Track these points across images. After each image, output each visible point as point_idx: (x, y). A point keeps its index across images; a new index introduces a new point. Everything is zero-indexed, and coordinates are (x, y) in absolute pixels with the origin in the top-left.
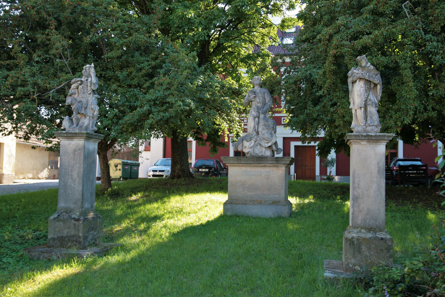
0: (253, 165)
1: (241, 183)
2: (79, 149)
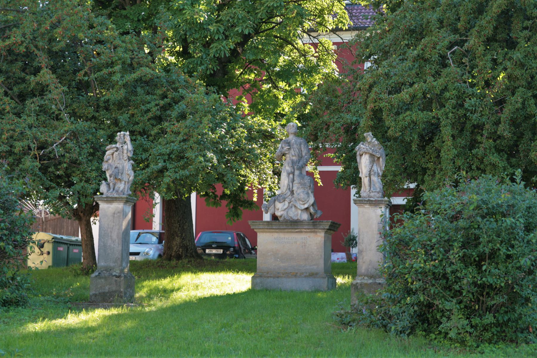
0: (286, 230)
2: (119, 212)
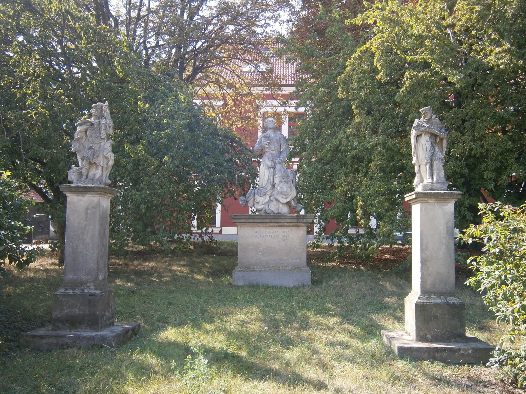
0: (268, 224)
1: (253, 247)
2: (93, 207)
